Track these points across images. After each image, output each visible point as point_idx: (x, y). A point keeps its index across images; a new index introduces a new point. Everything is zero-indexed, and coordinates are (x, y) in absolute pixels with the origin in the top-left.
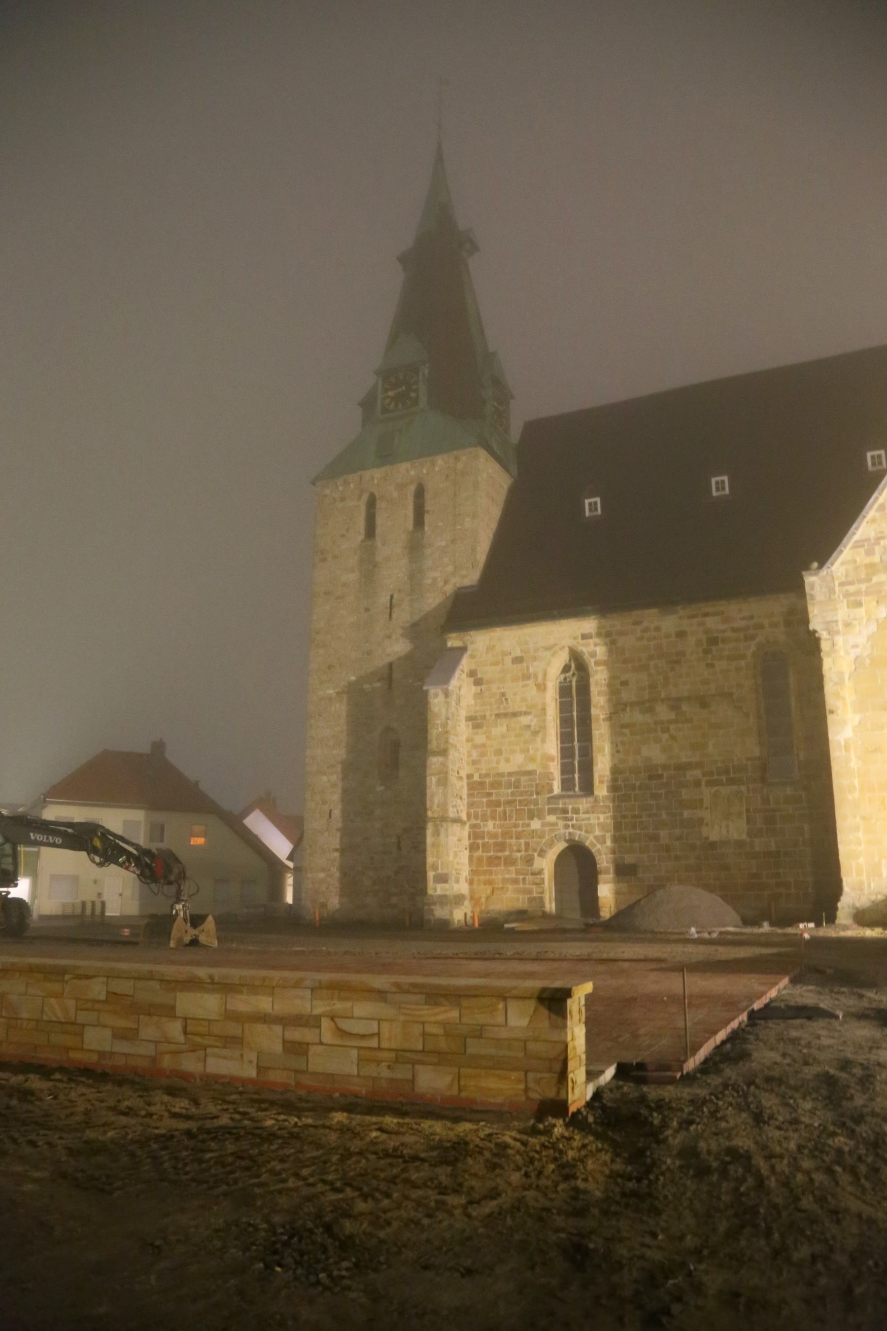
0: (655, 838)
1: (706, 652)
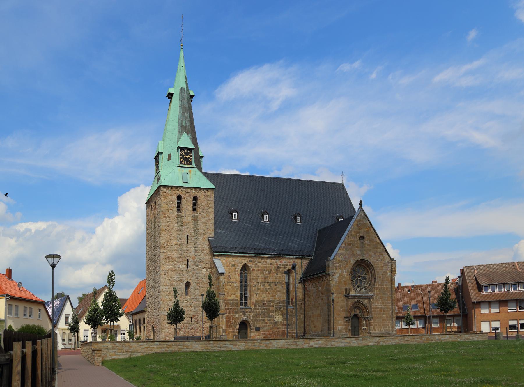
0: (264, 320)
1: (276, 270)
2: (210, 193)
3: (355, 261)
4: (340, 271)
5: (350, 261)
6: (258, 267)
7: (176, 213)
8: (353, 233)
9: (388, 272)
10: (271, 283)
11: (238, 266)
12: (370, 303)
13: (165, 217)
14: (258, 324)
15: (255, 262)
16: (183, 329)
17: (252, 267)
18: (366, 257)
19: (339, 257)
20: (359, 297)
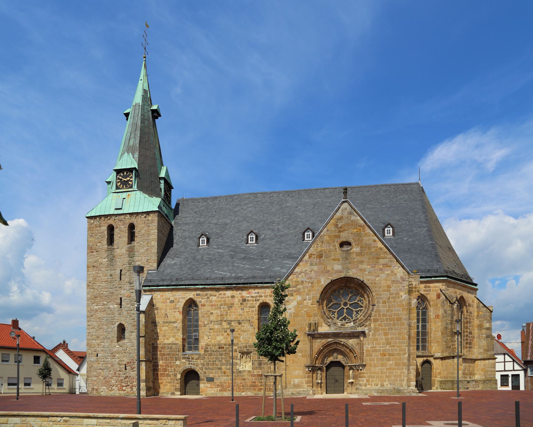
1: (241, 304)
2: (151, 217)
3: (329, 281)
4: (299, 298)
5: (319, 282)
6: (211, 301)
7: (106, 246)
8: (326, 238)
9: (402, 293)
10: (231, 321)
11: (179, 302)
12: (361, 345)
13: (92, 252)
14: (211, 373)
15: (206, 295)
16: (114, 378)
17: (200, 302)
18: (352, 273)
19: (297, 277)
20: (336, 335)
